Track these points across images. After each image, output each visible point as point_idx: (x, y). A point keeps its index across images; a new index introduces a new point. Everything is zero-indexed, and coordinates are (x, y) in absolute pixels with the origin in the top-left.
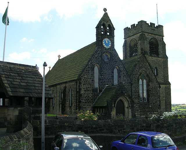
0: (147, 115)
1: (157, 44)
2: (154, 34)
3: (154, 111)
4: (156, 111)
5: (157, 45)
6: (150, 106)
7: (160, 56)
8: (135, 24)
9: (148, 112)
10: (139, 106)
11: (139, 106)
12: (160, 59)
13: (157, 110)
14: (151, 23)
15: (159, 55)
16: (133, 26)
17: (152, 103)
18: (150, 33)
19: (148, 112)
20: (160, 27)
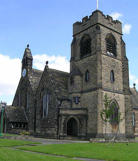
0: (45, 131)
1: (115, 42)
2: (82, 32)
3: (51, 127)
4: (53, 127)
5: (115, 43)
6: (49, 122)
7: (118, 57)
8: (87, 16)
9: (46, 128)
10: (40, 122)
11: (40, 122)
12: (117, 61)
13: (54, 126)
14: (107, 16)
15: (117, 55)
16: (86, 19)
17: (50, 118)
18: (80, 32)
19: (46, 128)
20: (77, 24)
